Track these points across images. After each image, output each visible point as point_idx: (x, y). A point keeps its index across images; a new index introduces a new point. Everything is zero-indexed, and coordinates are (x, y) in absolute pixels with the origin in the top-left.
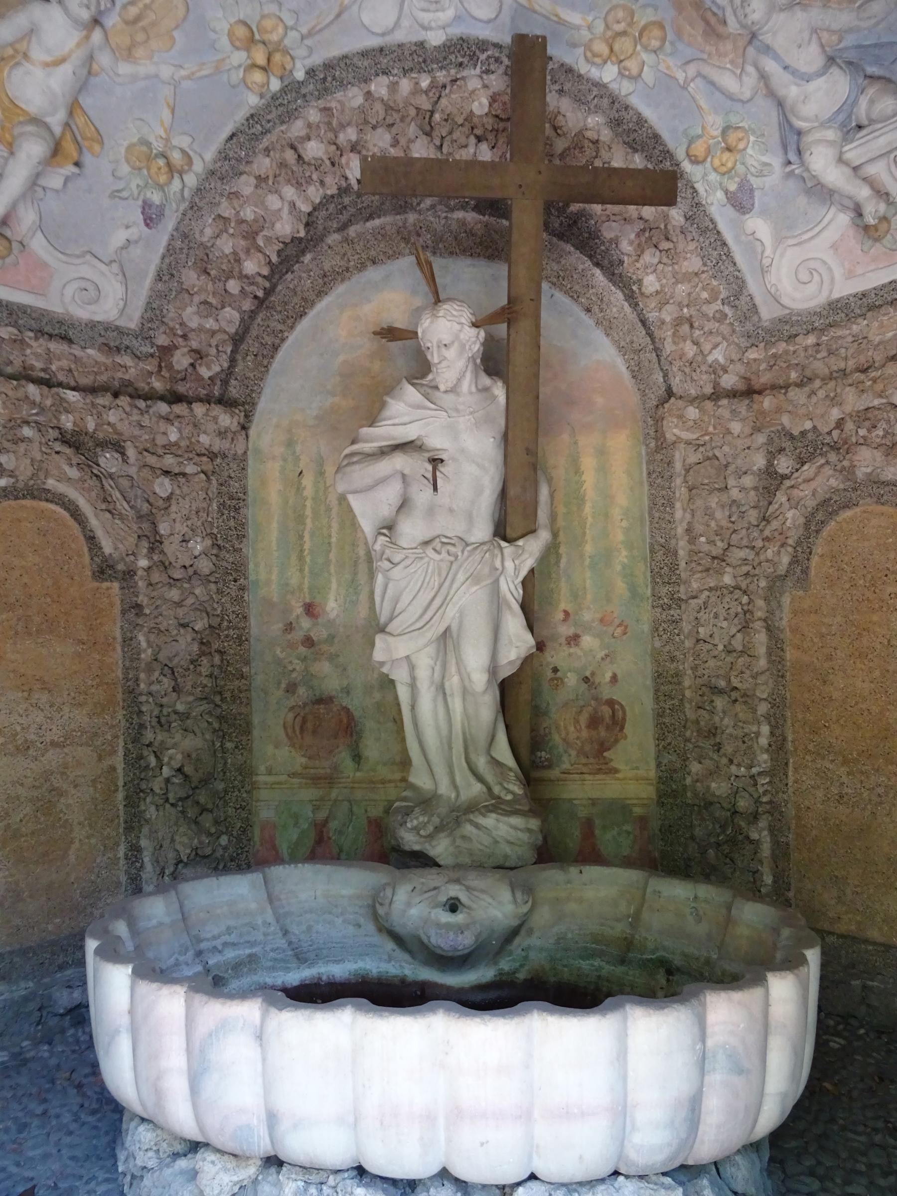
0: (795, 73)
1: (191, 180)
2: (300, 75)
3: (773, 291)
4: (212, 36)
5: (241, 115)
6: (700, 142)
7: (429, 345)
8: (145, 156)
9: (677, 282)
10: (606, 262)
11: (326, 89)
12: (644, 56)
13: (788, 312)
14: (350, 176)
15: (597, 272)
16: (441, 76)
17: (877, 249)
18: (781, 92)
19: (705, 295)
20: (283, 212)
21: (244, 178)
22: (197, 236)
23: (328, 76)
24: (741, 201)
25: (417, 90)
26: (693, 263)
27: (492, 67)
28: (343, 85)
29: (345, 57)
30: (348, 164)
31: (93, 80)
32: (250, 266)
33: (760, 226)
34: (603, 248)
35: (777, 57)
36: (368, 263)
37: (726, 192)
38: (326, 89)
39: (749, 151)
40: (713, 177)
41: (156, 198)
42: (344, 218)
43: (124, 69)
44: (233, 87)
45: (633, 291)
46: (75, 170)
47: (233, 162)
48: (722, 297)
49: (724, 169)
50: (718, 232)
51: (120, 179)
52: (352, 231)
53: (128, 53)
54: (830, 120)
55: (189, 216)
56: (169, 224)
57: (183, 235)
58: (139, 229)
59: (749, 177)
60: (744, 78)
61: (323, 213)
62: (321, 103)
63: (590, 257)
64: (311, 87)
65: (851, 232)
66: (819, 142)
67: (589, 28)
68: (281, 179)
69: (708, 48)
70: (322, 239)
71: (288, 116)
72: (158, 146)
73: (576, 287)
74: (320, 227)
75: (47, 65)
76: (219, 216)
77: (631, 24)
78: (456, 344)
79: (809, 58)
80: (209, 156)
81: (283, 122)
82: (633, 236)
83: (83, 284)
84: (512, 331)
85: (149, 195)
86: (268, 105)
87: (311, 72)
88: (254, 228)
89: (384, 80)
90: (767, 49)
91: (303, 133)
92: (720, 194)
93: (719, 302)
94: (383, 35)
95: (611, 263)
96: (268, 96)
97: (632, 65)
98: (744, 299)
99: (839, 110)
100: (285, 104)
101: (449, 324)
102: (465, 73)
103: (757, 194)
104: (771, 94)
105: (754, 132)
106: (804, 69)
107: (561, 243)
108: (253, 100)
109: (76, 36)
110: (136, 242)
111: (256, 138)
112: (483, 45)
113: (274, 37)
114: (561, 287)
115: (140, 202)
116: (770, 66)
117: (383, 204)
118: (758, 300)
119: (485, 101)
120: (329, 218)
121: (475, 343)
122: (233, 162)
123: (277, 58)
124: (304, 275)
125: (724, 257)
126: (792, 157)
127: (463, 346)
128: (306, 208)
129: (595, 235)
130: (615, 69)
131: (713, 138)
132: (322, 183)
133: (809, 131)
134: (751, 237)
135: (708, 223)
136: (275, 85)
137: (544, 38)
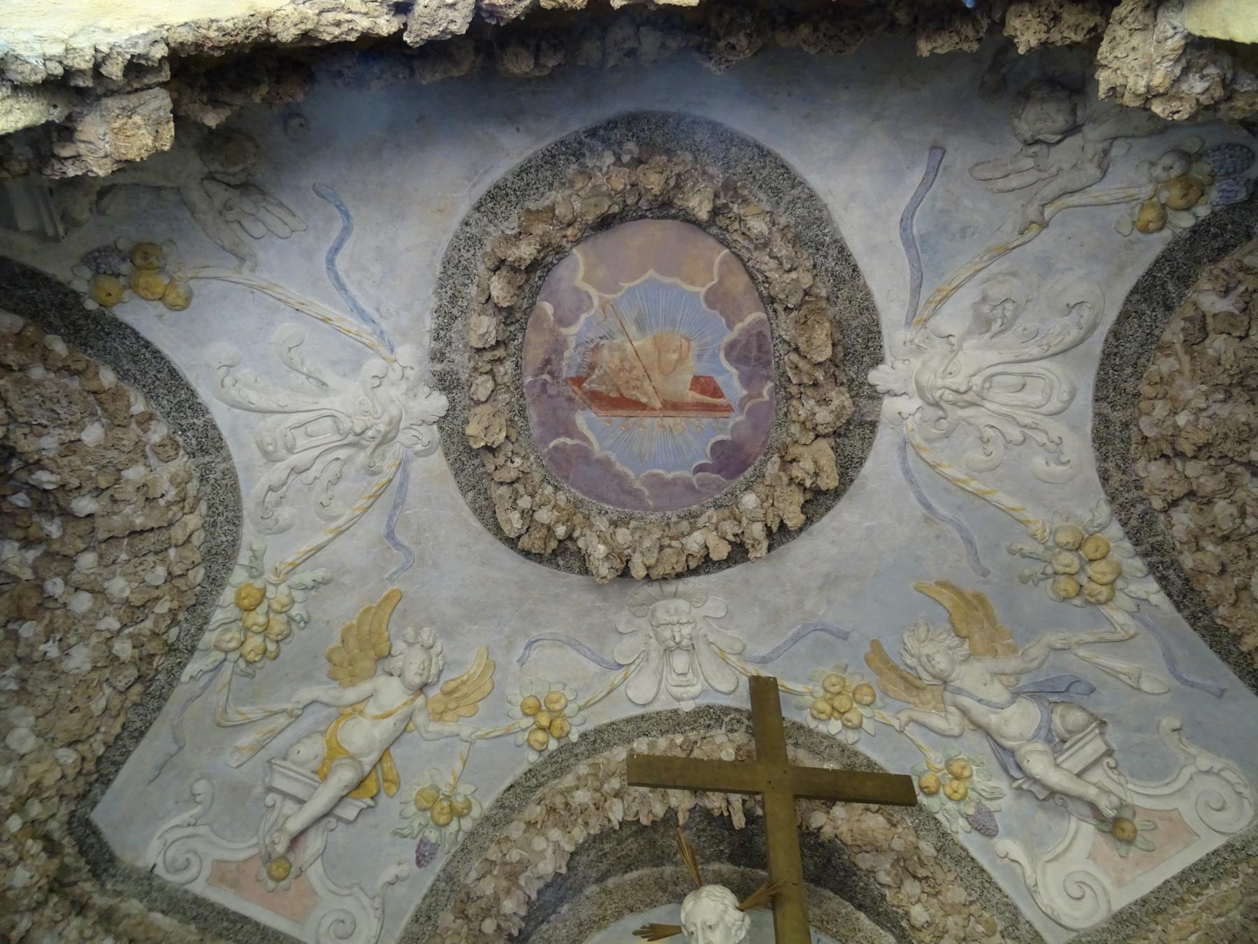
0: (988, 704)
1: (467, 824)
2: (574, 737)
3: (1049, 912)
4: (509, 706)
5: (524, 767)
6: (928, 775)
7: (693, 929)
8: (430, 801)
9: (947, 915)
10: (868, 901)
11: (595, 750)
12: (861, 711)
13: (1074, 934)
14: (612, 818)
15: (862, 915)
16: (692, 735)
17: (1134, 853)
18: (983, 720)
19: (980, 928)
20: (547, 853)
21: (514, 824)
22: (462, 879)
23: (597, 740)
24: (984, 826)
25: (672, 744)
26: (957, 894)
27: (735, 727)
28: (609, 745)
29: (613, 723)
30: (611, 808)
31: (406, 736)
32: (508, 906)
33: (1007, 845)
34: (861, 884)
35: (970, 695)
36: (626, 912)
37: (967, 817)
38: (595, 750)
39: (975, 778)
40: (950, 805)
41: (432, 836)
42: (603, 866)
43: (434, 727)
44: (518, 746)
45: (903, 929)
46: (371, 803)
47: (507, 810)
48: (999, 928)
49: (957, 796)
50: (973, 859)
51: (406, 818)
52: (610, 883)
53: (440, 716)
54: (1035, 736)
55: (458, 858)
56: (438, 865)
57: (448, 877)
58: (410, 867)
59: (984, 802)
60: (950, 717)
61: (584, 859)
62: (590, 761)
63: (851, 900)
64: (583, 748)
65: (1101, 839)
66: (1031, 752)
67: (811, 694)
68: (549, 823)
69: (911, 700)
70: (580, 890)
71: (562, 771)
72: (446, 790)
73: (843, 931)
74: (581, 875)
75: (376, 717)
76: (486, 860)
77: (844, 687)
78: (721, 926)
79: (997, 692)
80: (487, 804)
81: (556, 777)
82: (888, 866)
83: (343, 916)
84: (779, 916)
85: (427, 833)
86: (545, 762)
87: (584, 736)
88: (518, 869)
89: (645, 740)
90: (959, 691)
91: (573, 784)
92: (962, 822)
93: (998, 935)
94: (644, 705)
95: (874, 901)
96: (546, 753)
97: (853, 717)
98: (1023, 928)
99: (1040, 728)
100: (559, 762)
101: (712, 904)
102: (713, 732)
103: (996, 816)
104: (978, 727)
105: (974, 762)
106: (995, 700)
107: (819, 889)
108: (533, 757)
109: (406, 698)
110: (404, 880)
111: (532, 790)
112: (726, 710)
113: (558, 707)
114: (826, 931)
115: (417, 841)
116: (967, 702)
117: (641, 853)
118: (1038, 926)
119: (732, 751)
120: (589, 865)
121: (740, 929)
122: (507, 810)
123: (558, 722)
124: (560, 925)
125: (987, 885)
126: (1016, 774)
127: (728, 929)
128: (570, 848)
129: (851, 871)
130: (839, 723)
131: (940, 770)
132: (586, 824)
133: (1020, 746)
134: (1006, 860)
135: (959, 851)
136: (553, 745)
137: (775, 679)
